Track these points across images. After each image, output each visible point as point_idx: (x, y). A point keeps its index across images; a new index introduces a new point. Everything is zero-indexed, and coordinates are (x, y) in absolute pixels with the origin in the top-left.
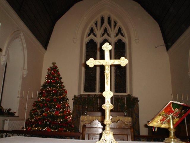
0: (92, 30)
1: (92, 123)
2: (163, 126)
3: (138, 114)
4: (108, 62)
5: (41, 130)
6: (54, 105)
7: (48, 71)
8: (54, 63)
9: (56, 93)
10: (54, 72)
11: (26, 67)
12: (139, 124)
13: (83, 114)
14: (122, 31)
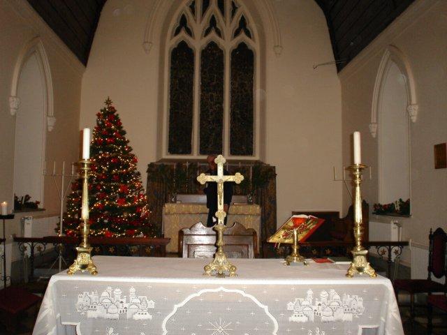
0: (183, 21)
1: (193, 228)
2: (287, 241)
3: (276, 197)
4: (220, 177)
5: (94, 234)
6: (115, 187)
7: (96, 117)
8: (108, 102)
9: (117, 164)
10: (110, 120)
11: (51, 112)
12: (275, 218)
13: (166, 201)
14: (247, 25)
